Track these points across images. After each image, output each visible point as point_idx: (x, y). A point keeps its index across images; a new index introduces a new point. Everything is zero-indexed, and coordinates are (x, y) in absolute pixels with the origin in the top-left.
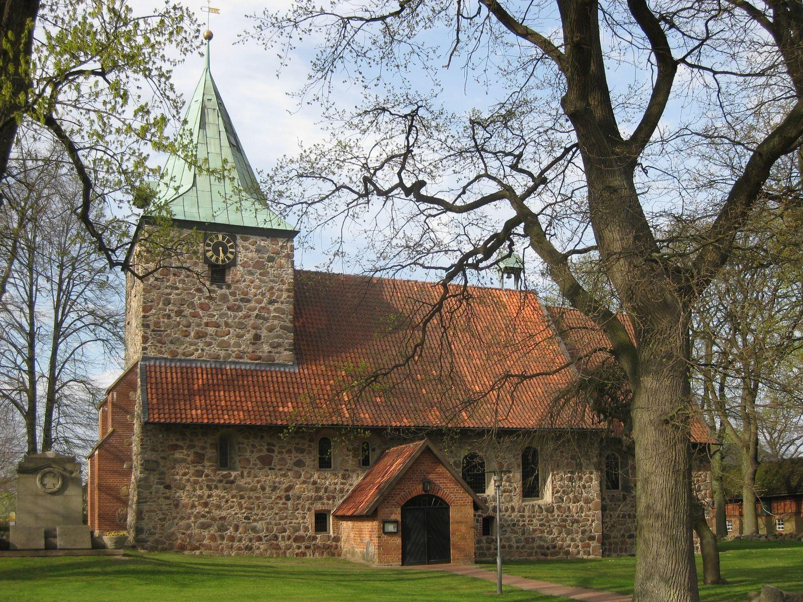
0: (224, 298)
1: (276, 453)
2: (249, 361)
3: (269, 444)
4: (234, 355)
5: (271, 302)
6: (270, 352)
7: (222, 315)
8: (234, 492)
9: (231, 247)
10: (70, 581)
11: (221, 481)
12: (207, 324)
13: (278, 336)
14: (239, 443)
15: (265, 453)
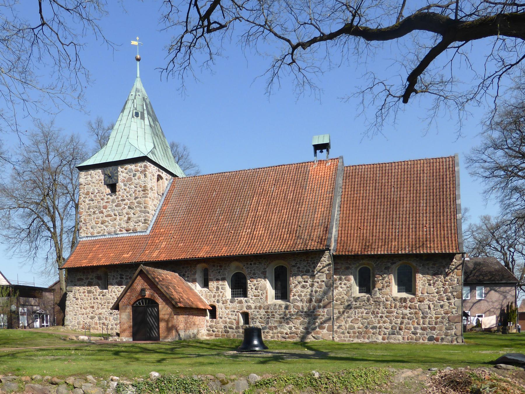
3: (121, 275)
10: (299, 363)
15: (119, 279)
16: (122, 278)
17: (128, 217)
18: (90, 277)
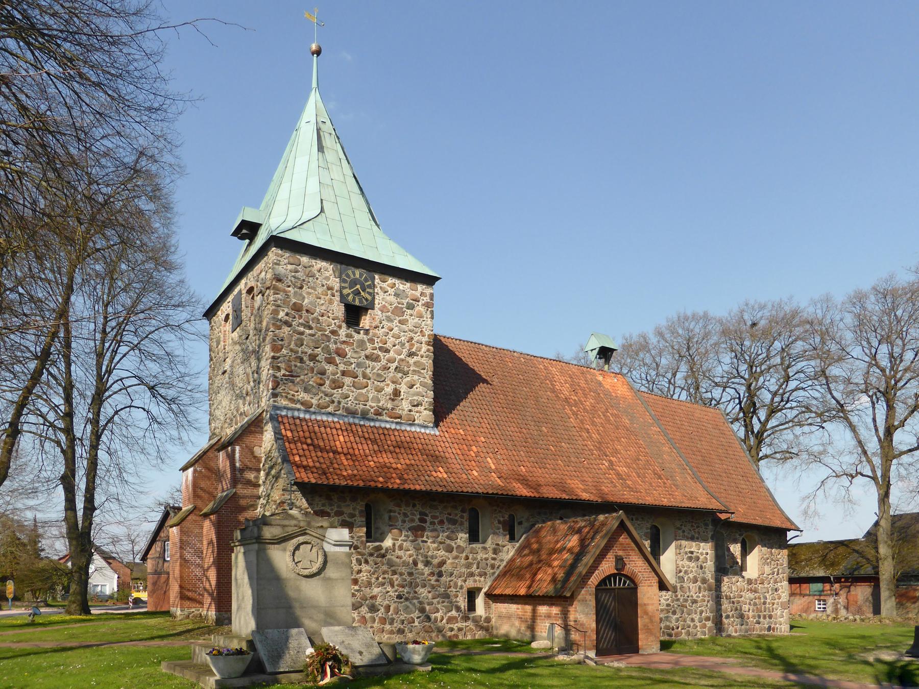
0: (361, 343)
1: (428, 524)
2: (388, 419)
3: (421, 514)
4: (372, 410)
5: (411, 354)
6: (410, 411)
7: (359, 365)
8: (385, 568)
9: (369, 287)
11: (371, 555)
12: (344, 373)
13: (418, 394)
14: (391, 511)
16: (424, 521)
17: (395, 389)
18: (348, 510)
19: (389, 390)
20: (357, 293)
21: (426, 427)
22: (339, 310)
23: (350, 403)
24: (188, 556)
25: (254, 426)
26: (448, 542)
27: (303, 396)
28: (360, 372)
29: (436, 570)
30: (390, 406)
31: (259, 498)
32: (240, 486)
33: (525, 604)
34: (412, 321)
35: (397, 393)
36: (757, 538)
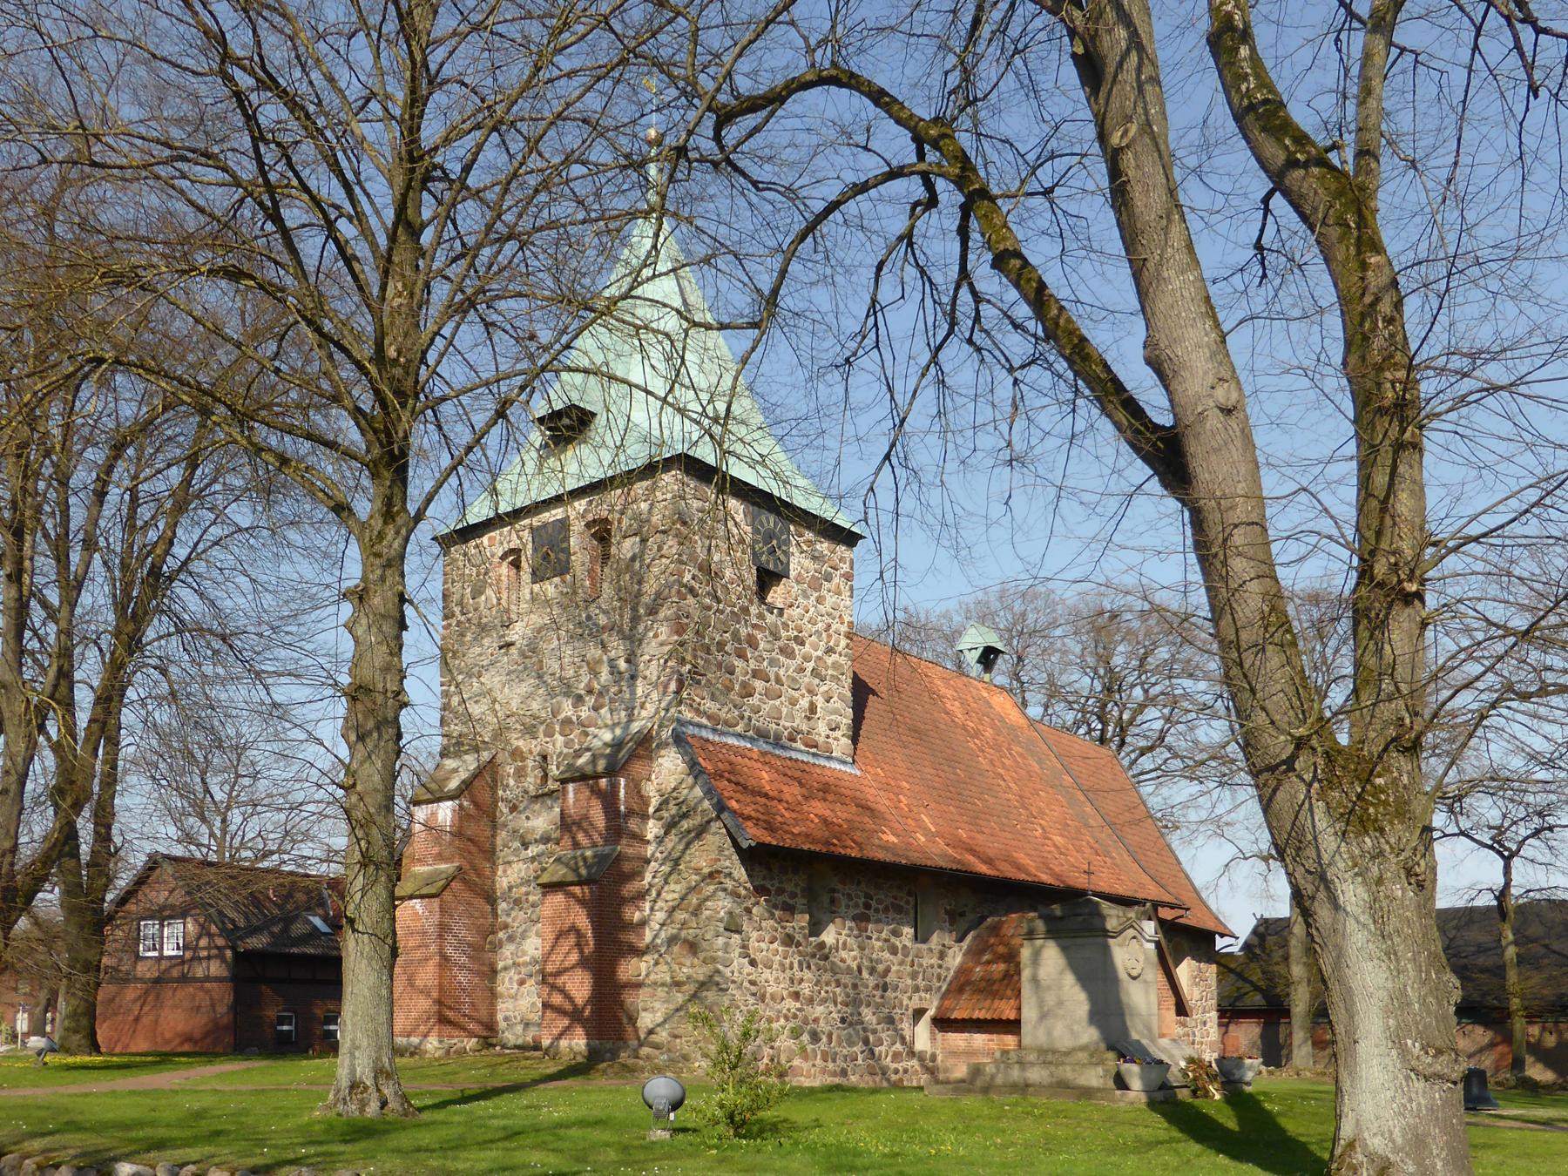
11: (814, 956)
18: (790, 887)
19: (804, 703)
20: (772, 551)
21: (844, 763)
22: (751, 578)
23: (759, 722)
24: (449, 951)
25: (644, 746)
26: (893, 939)
27: (708, 705)
28: (772, 672)
29: (881, 981)
30: (805, 728)
31: (648, 862)
32: (624, 842)
33: (1006, 1033)
34: (830, 600)
35: (813, 708)
36: (1186, 946)
